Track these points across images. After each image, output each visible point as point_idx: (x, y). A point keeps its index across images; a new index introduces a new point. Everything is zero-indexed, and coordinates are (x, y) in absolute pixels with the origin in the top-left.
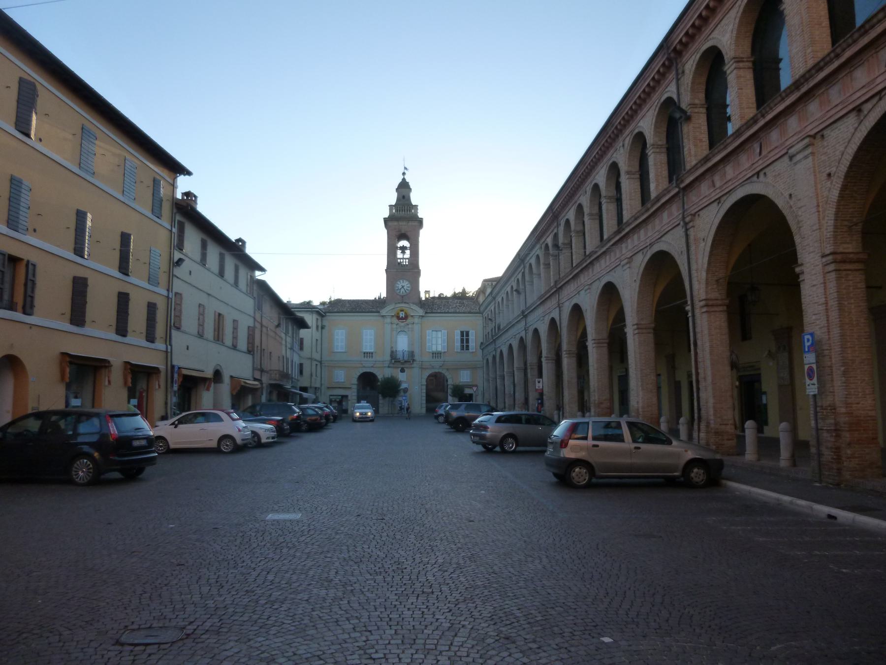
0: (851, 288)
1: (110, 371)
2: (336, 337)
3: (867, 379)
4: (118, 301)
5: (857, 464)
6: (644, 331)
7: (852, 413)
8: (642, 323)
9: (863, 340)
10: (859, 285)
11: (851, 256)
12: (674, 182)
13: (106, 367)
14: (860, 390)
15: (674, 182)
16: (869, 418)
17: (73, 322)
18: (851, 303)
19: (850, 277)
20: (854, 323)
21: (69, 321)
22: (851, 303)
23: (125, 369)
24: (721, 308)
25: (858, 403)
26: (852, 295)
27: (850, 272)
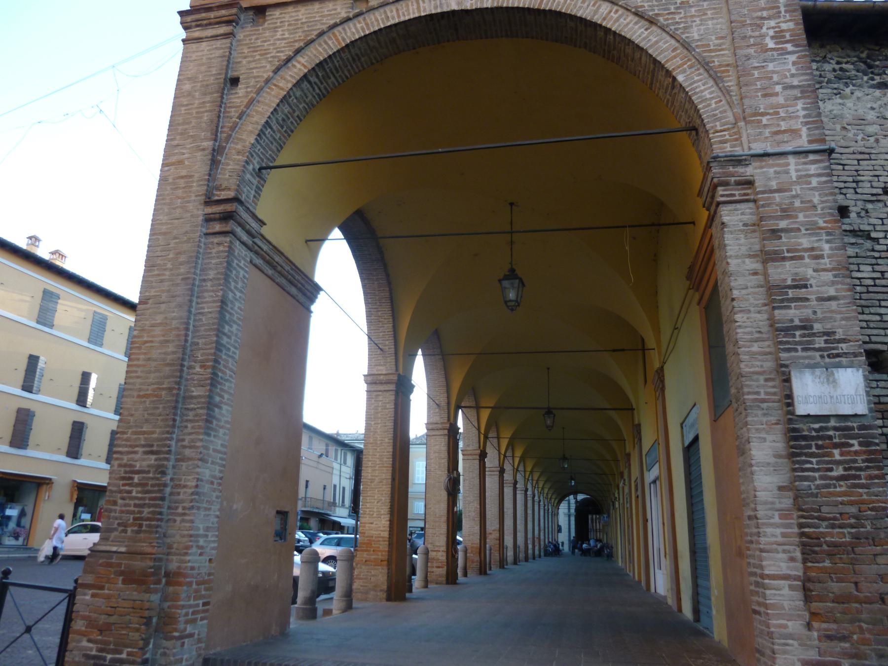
0: (380, 408)
1: (51, 487)
2: (417, 469)
3: (383, 499)
4: (72, 429)
5: (361, 586)
6: (470, 457)
7: (364, 533)
8: (468, 449)
9: (385, 459)
10: (388, 406)
11: (382, 377)
12: (800, 240)
13: (48, 484)
14: (375, 510)
15: (800, 240)
16: (381, 539)
17: (12, 444)
18: (378, 424)
19: (380, 398)
20: (379, 442)
21: (9, 444)
22: (378, 424)
23: (73, 487)
24: (441, 432)
25: (372, 523)
26: (379, 415)
27: (380, 393)
